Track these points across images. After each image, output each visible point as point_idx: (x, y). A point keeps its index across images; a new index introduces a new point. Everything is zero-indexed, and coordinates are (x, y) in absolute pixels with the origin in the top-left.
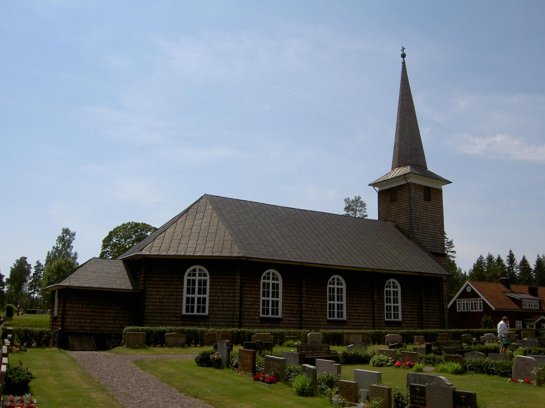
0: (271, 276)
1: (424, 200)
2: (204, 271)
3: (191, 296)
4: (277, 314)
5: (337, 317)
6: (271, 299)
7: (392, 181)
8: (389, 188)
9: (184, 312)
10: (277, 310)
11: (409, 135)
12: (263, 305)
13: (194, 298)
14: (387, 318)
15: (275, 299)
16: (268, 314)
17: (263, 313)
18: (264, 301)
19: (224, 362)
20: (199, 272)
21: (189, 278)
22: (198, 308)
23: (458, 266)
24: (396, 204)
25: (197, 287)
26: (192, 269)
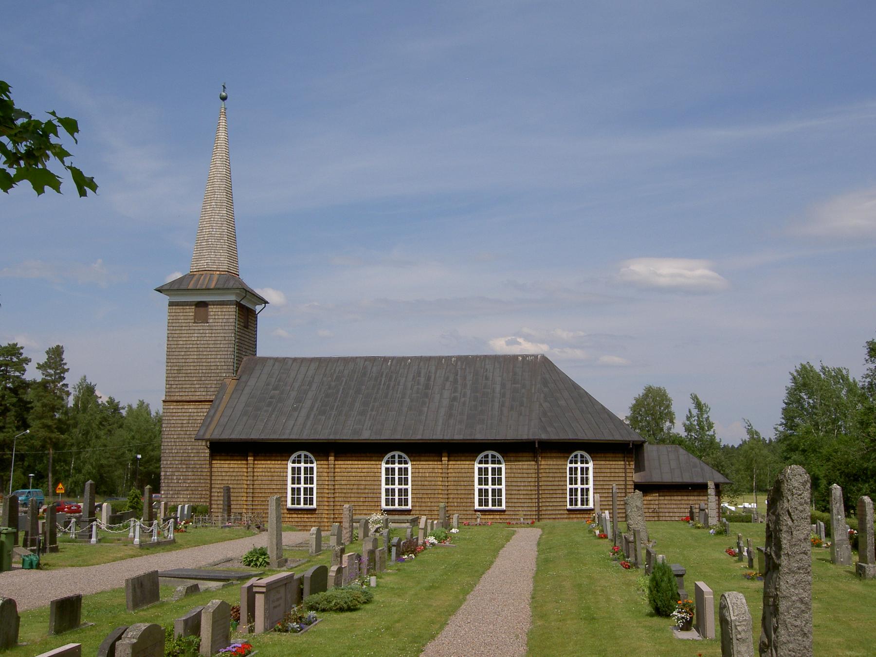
2: (404, 458)
5: (399, 505)
9: (289, 505)
11: (244, 337)
12: (571, 495)
16: (299, 504)
18: (571, 489)
19: (272, 554)
21: (388, 466)
22: (400, 500)
25: (302, 476)
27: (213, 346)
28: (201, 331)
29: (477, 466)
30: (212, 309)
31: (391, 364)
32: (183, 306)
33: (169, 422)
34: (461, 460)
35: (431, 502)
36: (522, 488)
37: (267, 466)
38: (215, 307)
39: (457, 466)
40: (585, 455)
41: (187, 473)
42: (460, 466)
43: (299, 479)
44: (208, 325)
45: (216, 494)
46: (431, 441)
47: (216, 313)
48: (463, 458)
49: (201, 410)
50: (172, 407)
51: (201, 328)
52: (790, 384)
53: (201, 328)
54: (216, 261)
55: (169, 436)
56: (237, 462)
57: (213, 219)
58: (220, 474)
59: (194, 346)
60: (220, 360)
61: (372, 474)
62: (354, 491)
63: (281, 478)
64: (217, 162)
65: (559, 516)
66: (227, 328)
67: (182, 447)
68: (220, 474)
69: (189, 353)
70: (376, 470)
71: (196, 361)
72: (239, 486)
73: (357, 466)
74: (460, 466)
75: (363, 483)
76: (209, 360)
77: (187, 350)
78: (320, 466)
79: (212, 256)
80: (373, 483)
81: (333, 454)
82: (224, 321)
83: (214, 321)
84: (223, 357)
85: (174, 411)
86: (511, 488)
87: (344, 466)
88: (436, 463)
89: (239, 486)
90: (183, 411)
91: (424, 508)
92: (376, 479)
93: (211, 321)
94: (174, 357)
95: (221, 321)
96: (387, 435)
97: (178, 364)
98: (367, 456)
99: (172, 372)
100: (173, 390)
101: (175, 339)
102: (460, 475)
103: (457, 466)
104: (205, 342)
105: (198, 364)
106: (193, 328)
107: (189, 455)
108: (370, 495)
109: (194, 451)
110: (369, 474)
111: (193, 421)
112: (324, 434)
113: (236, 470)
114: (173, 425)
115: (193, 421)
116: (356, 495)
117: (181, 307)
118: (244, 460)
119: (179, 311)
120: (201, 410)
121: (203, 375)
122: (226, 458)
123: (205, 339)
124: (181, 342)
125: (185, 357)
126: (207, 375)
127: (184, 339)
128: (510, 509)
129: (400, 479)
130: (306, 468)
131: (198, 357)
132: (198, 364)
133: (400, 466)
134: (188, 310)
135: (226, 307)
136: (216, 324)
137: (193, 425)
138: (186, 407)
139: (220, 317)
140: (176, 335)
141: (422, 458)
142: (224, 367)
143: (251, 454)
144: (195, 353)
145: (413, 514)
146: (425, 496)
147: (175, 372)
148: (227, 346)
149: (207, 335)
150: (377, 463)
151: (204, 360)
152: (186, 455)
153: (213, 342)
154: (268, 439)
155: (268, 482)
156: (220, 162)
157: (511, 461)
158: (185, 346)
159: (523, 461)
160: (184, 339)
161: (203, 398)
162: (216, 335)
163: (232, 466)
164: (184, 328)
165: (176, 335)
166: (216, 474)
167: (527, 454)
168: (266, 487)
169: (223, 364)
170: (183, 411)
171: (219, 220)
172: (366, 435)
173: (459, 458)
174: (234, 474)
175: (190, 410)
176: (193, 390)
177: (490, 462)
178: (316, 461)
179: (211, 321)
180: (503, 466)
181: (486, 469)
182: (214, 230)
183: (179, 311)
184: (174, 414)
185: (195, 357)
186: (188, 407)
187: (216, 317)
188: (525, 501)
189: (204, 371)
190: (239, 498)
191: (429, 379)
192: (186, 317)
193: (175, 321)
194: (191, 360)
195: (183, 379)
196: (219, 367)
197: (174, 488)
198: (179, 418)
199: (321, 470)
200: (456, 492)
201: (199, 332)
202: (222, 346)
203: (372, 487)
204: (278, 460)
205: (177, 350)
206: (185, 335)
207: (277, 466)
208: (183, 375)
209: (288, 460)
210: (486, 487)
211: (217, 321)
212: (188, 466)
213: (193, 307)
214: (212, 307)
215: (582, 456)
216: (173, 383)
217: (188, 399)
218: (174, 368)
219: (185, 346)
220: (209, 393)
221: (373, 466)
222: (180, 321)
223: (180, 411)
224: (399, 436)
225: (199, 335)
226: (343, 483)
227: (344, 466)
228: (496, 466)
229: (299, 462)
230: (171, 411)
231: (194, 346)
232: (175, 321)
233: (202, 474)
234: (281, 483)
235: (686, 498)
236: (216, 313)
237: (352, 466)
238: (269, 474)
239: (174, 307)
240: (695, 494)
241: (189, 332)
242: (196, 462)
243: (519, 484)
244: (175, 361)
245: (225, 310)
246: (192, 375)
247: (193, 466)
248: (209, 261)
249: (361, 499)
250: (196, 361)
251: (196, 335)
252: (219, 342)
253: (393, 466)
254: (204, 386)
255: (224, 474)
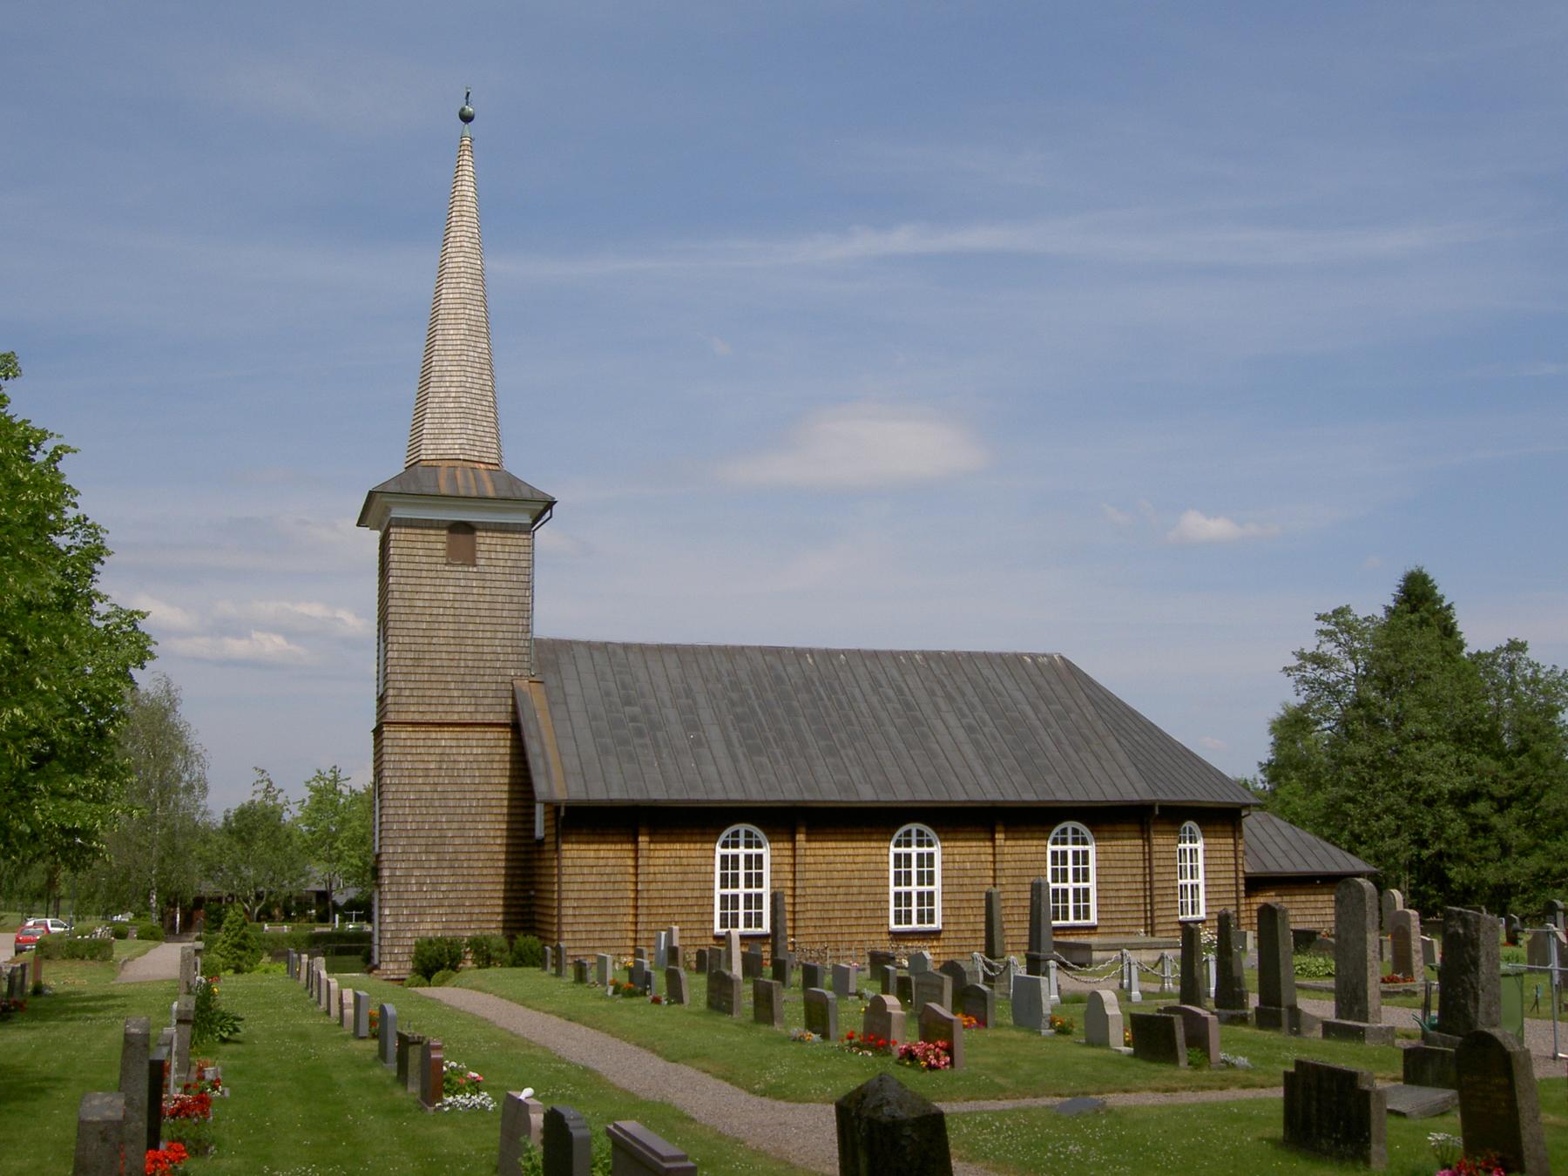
2: (756, 837)
3: (729, 891)
4: (1087, 917)
6: (1070, 885)
10: (1087, 909)
13: (737, 896)
14: (896, 923)
15: (1081, 885)
17: (898, 922)
21: (899, 850)
23: (1272, 739)
25: (742, 872)
27: (487, 613)
28: (463, 583)
29: (893, 850)
30: (484, 540)
31: (814, 661)
32: (422, 528)
33: (397, 765)
34: (1024, 839)
35: (975, 915)
36: (1123, 886)
37: (674, 854)
38: (490, 534)
39: (1017, 850)
40: (1081, 830)
41: (440, 872)
42: (1022, 850)
43: (736, 877)
44: (475, 569)
45: (570, 912)
46: (745, 805)
47: (492, 548)
48: (1027, 835)
49: (467, 743)
50: (403, 735)
51: (462, 575)
52: (178, 708)
53: (462, 575)
54: (477, 443)
55: (399, 796)
56: (613, 847)
57: (465, 358)
58: (577, 870)
59: (448, 611)
60: (503, 642)
61: (872, 866)
62: (839, 898)
63: (701, 877)
64: (465, 244)
65: (1116, 930)
66: (515, 578)
67: (428, 818)
68: (577, 870)
69: (436, 626)
70: (879, 859)
71: (452, 641)
72: (620, 894)
73: (844, 852)
74: (1022, 850)
75: (856, 882)
76: (480, 642)
77: (433, 618)
78: (776, 853)
79: (468, 432)
80: (874, 882)
81: (803, 829)
82: (509, 563)
83: (489, 562)
84: (509, 635)
85: (409, 743)
86: (1104, 886)
87: (821, 852)
88: (982, 844)
89: (620, 894)
90: (430, 743)
91: (963, 927)
92: (878, 874)
93: (482, 562)
94: (405, 632)
95: (502, 563)
96: (902, 794)
97: (413, 647)
98: (862, 833)
99: (402, 662)
100: (404, 700)
101: (406, 595)
102: (1023, 865)
103: (1017, 850)
104: (471, 605)
105: (458, 649)
106: (447, 575)
107: (444, 833)
108: (869, 906)
109: (455, 825)
110: (867, 866)
111: (451, 765)
112: (788, 791)
113: (612, 862)
114: (406, 773)
115: (451, 765)
116: (843, 906)
117: (418, 531)
118: (628, 842)
119: (413, 538)
120: (467, 743)
121: (467, 671)
122: (591, 838)
123: (470, 598)
124: (420, 603)
125: (427, 633)
126: (475, 671)
127: (427, 596)
128: (1103, 923)
129: (748, 877)
130: (920, 856)
131: (457, 634)
132: (458, 649)
133: (921, 850)
134: (433, 538)
135: (512, 536)
136: (492, 569)
137: (450, 772)
138: (434, 735)
139: (501, 556)
140: (409, 588)
141: (960, 836)
142: (511, 657)
143: (642, 830)
144: (451, 626)
145: (944, 939)
146: (965, 904)
147: (409, 662)
148: (516, 614)
149: (475, 591)
150: (881, 844)
151: (470, 642)
152: (437, 833)
153: (486, 606)
154: (689, 801)
155: (677, 886)
156: (469, 245)
157: (1104, 839)
158: (428, 611)
159: (1123, 839)
160: (427, 596)
161: (467, 718)
162: (494, 591)
163: (602, 854)
164: (424, 574)
165: (409, 588)
166: (570, 870)
167: (1127, 827)
168: (672, 894)
169: (510, 650)
170: (430, 743)
171: (477, 360)
172: (867, 794)
173: (1020, 835)
174: (608, 870)
175: (443, 743)
176: (447, 701)
177: (1070, 840)
178: (770, 842)
179: (482, 562)
180: (1091, 849)
181: (735, 858)
182: (470, 380)
183: (413, 538)
184: (408, 750)
185: (451, 634)
186: (439, 735)
187: (493, 555)
188: (1128, 908)
189: (470, 664)
190: (619, 919)
191: (900, 691)
192: (429, 552)
193: (405, 558)
194: (442, 641)
195: (426, 677)
196: (502, 657)
197: (411, 903)
198: (419, 758)
199: (778, 860)
200: (1015, 895)
201: (457, 583)
202: (505, 614)
203: (873, 890)
204: (696, 842)
205: (412, 618)
206: (428, 589)
207: (694, 854)
208: (426, 670)
209: (716, 842)
210: (1065, 886)
211: (494, 562)
212: (441, 856)
213: (445, 532)
214: (484, 534)
215: (1075, 831)
216: (403, 685)
217: (436, 718)
218: (404, 655)
219: (428, 611)
220: (481, 709)
221: (874, 852)
222: (417, 558)
223: (421, 743)
224: (924, 794)
225: (458, 590)
226: (820, 883)
227: (821, 852)
228: (1080, 848)
229: (908, 844)
230: (402, 743)
231: (448, 611)
232: (405, 558)
233: (471, 872)
234: (702, 885)
235: (1312, 898)
236: (492, 548)
237: (836, 852)
238: (678, 869)
239: (403, 530)
240: (1325, 890)
241: (438, 582)
242: (459, 848)
243: (1118, 879)
244: (407, 640)
245: (509, 542)
246: (446, 670)
247: (453, 856)
248: (465, 441)
249: (854, 914)
250: (452, 641)
251: (451, 589)
252: (499, 606)
253: (735, 851)
254: (470, 694)
255: (586, 870)
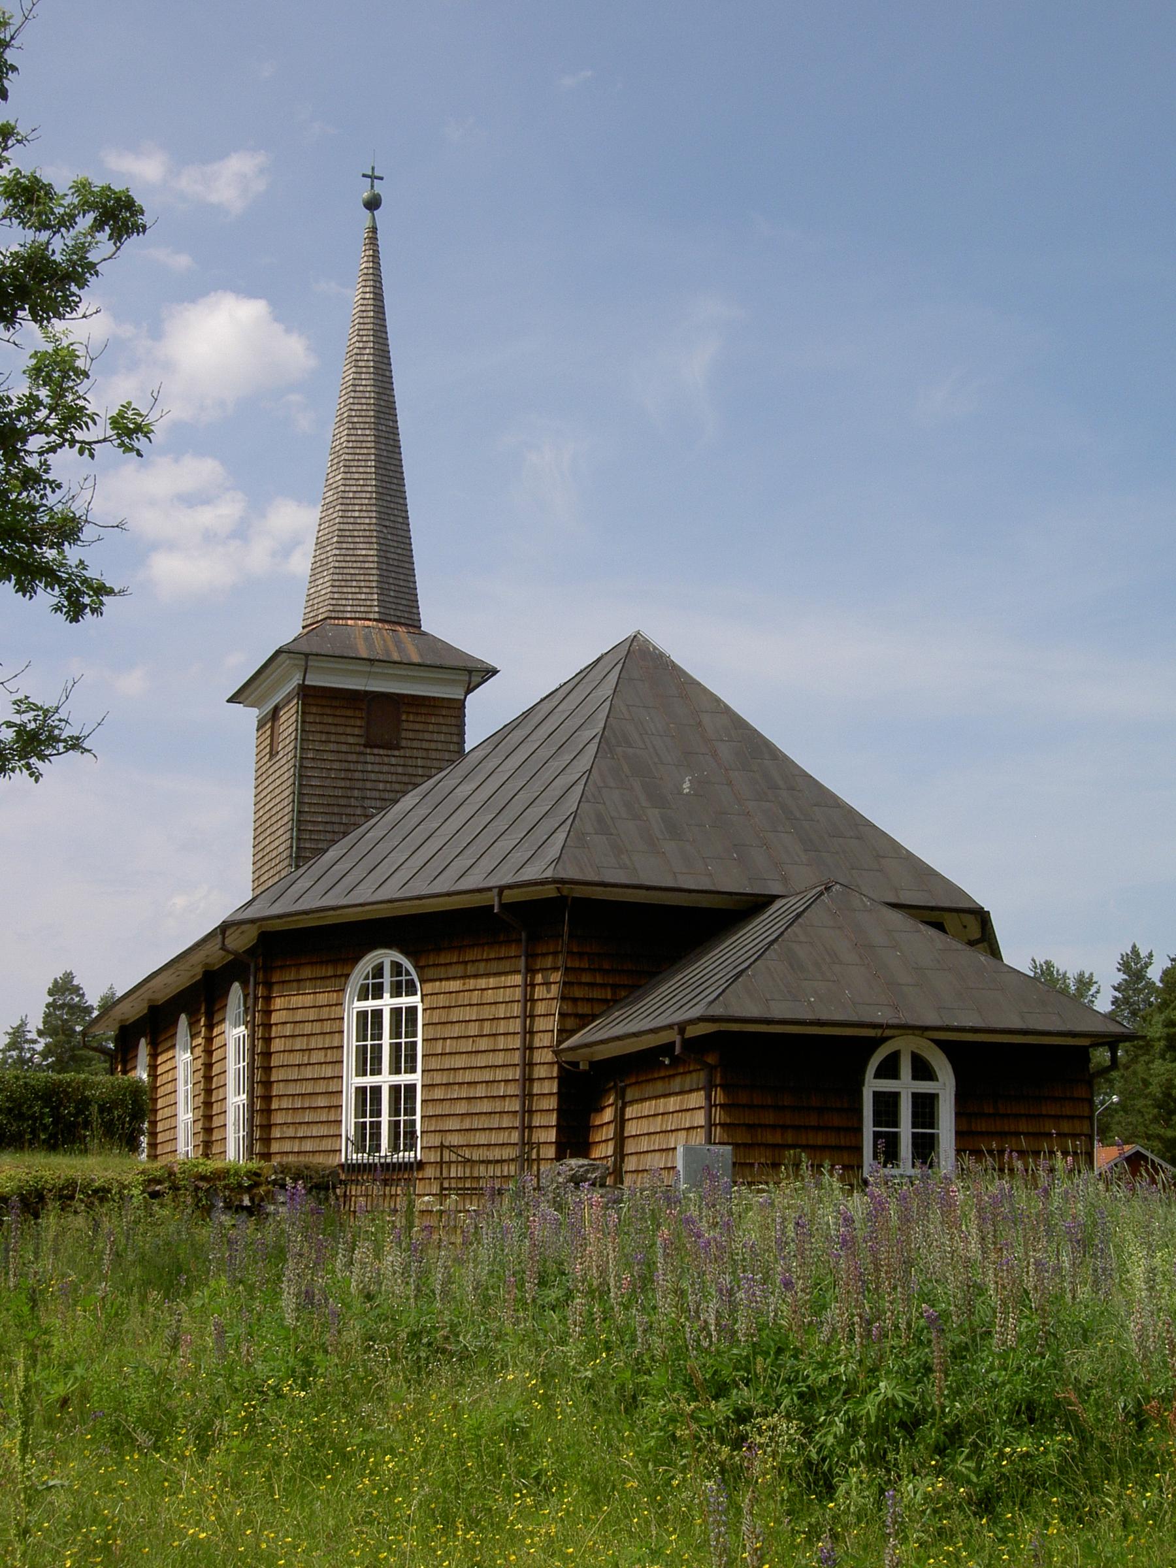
0: (387, 980)
1: (365, 746)
6: (385, 1079)
7: (351, 667)
8: (363, 688)
20: (390, 979)
24: (393, 761)
26: (372, 966)
